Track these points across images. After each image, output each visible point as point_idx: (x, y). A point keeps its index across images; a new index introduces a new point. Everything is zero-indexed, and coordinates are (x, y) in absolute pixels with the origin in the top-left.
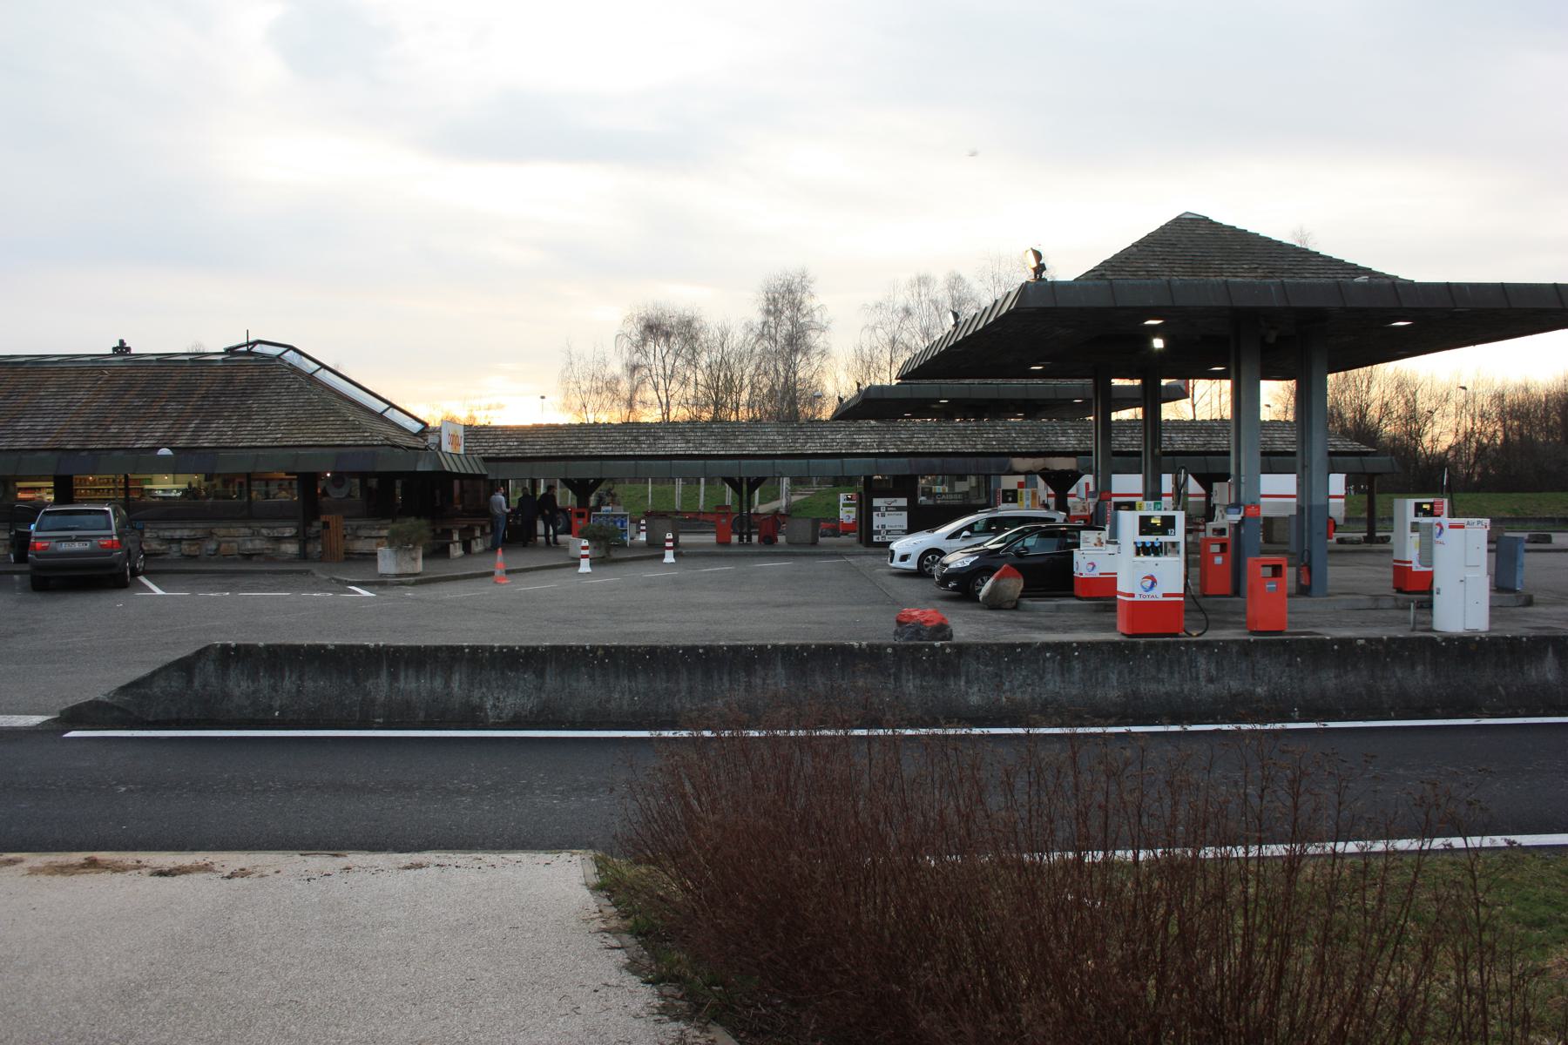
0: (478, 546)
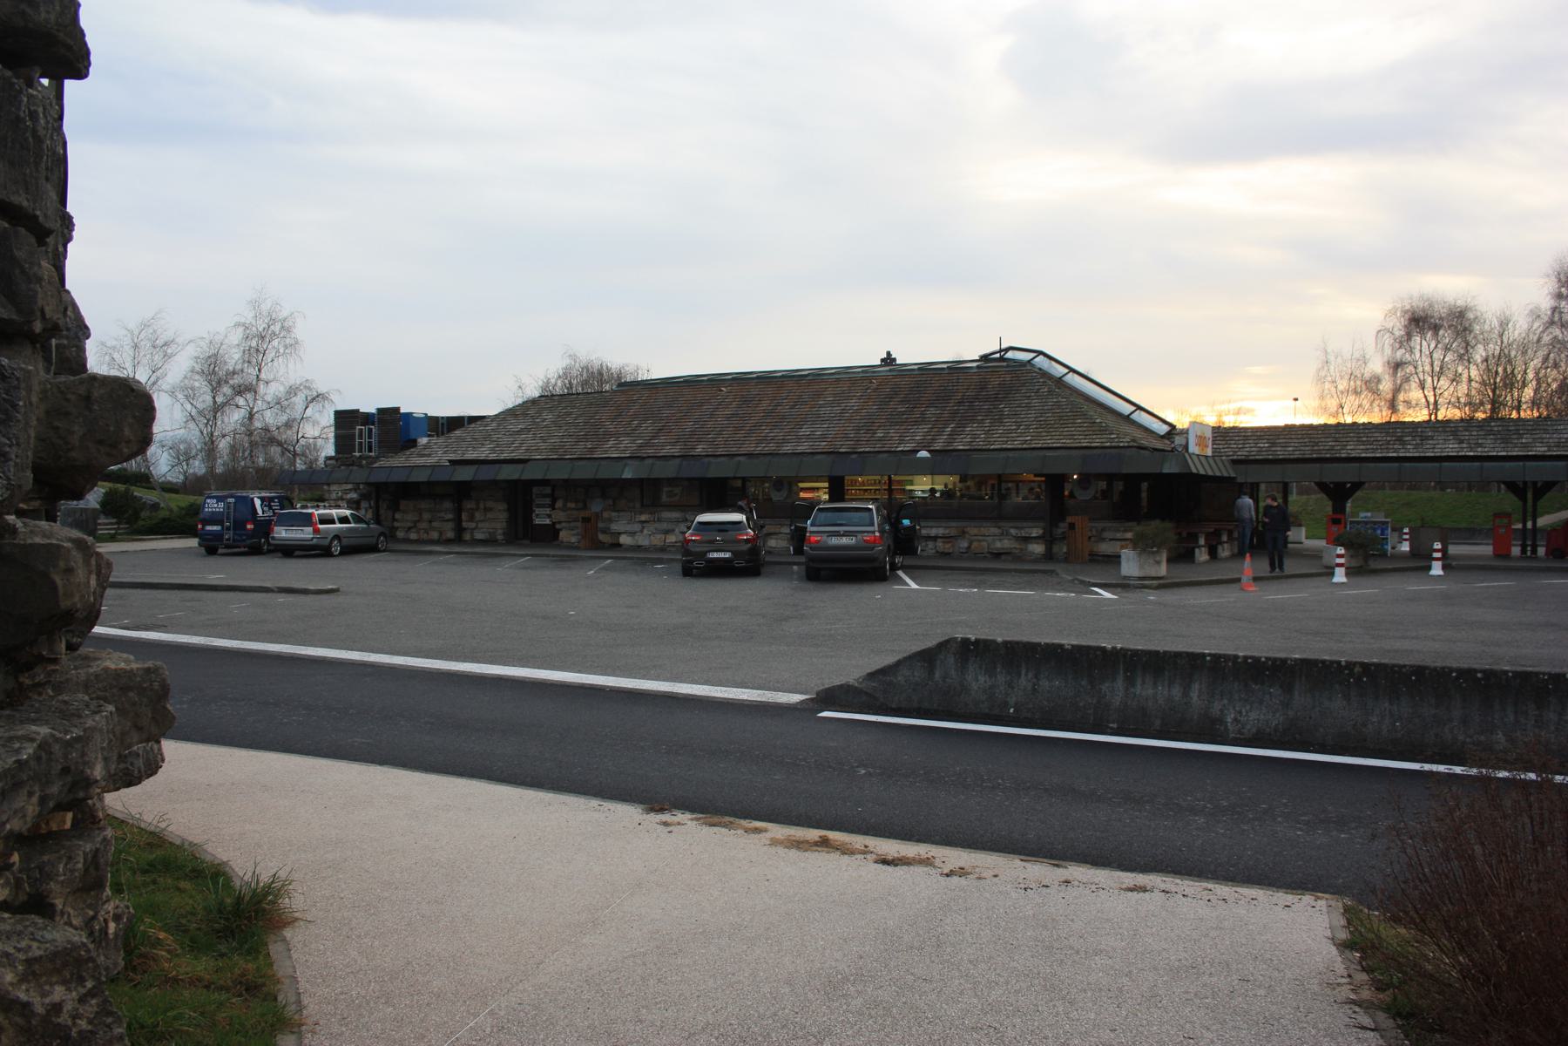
0: (1224, 551)
